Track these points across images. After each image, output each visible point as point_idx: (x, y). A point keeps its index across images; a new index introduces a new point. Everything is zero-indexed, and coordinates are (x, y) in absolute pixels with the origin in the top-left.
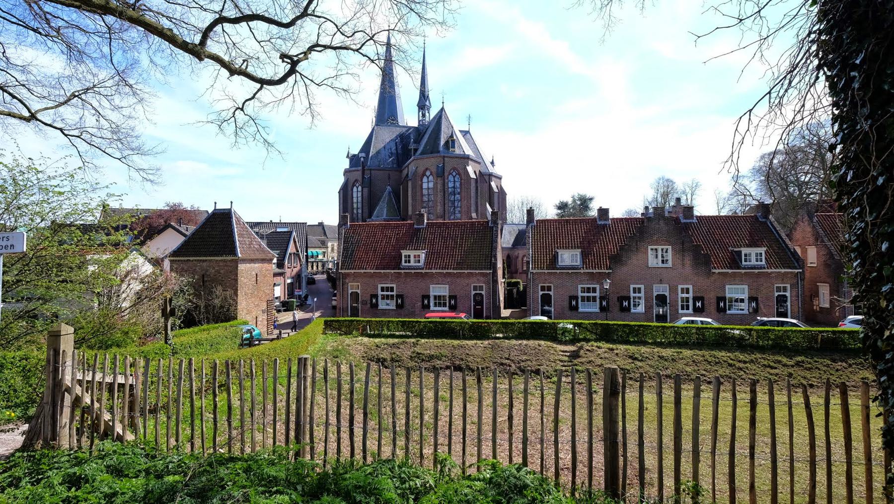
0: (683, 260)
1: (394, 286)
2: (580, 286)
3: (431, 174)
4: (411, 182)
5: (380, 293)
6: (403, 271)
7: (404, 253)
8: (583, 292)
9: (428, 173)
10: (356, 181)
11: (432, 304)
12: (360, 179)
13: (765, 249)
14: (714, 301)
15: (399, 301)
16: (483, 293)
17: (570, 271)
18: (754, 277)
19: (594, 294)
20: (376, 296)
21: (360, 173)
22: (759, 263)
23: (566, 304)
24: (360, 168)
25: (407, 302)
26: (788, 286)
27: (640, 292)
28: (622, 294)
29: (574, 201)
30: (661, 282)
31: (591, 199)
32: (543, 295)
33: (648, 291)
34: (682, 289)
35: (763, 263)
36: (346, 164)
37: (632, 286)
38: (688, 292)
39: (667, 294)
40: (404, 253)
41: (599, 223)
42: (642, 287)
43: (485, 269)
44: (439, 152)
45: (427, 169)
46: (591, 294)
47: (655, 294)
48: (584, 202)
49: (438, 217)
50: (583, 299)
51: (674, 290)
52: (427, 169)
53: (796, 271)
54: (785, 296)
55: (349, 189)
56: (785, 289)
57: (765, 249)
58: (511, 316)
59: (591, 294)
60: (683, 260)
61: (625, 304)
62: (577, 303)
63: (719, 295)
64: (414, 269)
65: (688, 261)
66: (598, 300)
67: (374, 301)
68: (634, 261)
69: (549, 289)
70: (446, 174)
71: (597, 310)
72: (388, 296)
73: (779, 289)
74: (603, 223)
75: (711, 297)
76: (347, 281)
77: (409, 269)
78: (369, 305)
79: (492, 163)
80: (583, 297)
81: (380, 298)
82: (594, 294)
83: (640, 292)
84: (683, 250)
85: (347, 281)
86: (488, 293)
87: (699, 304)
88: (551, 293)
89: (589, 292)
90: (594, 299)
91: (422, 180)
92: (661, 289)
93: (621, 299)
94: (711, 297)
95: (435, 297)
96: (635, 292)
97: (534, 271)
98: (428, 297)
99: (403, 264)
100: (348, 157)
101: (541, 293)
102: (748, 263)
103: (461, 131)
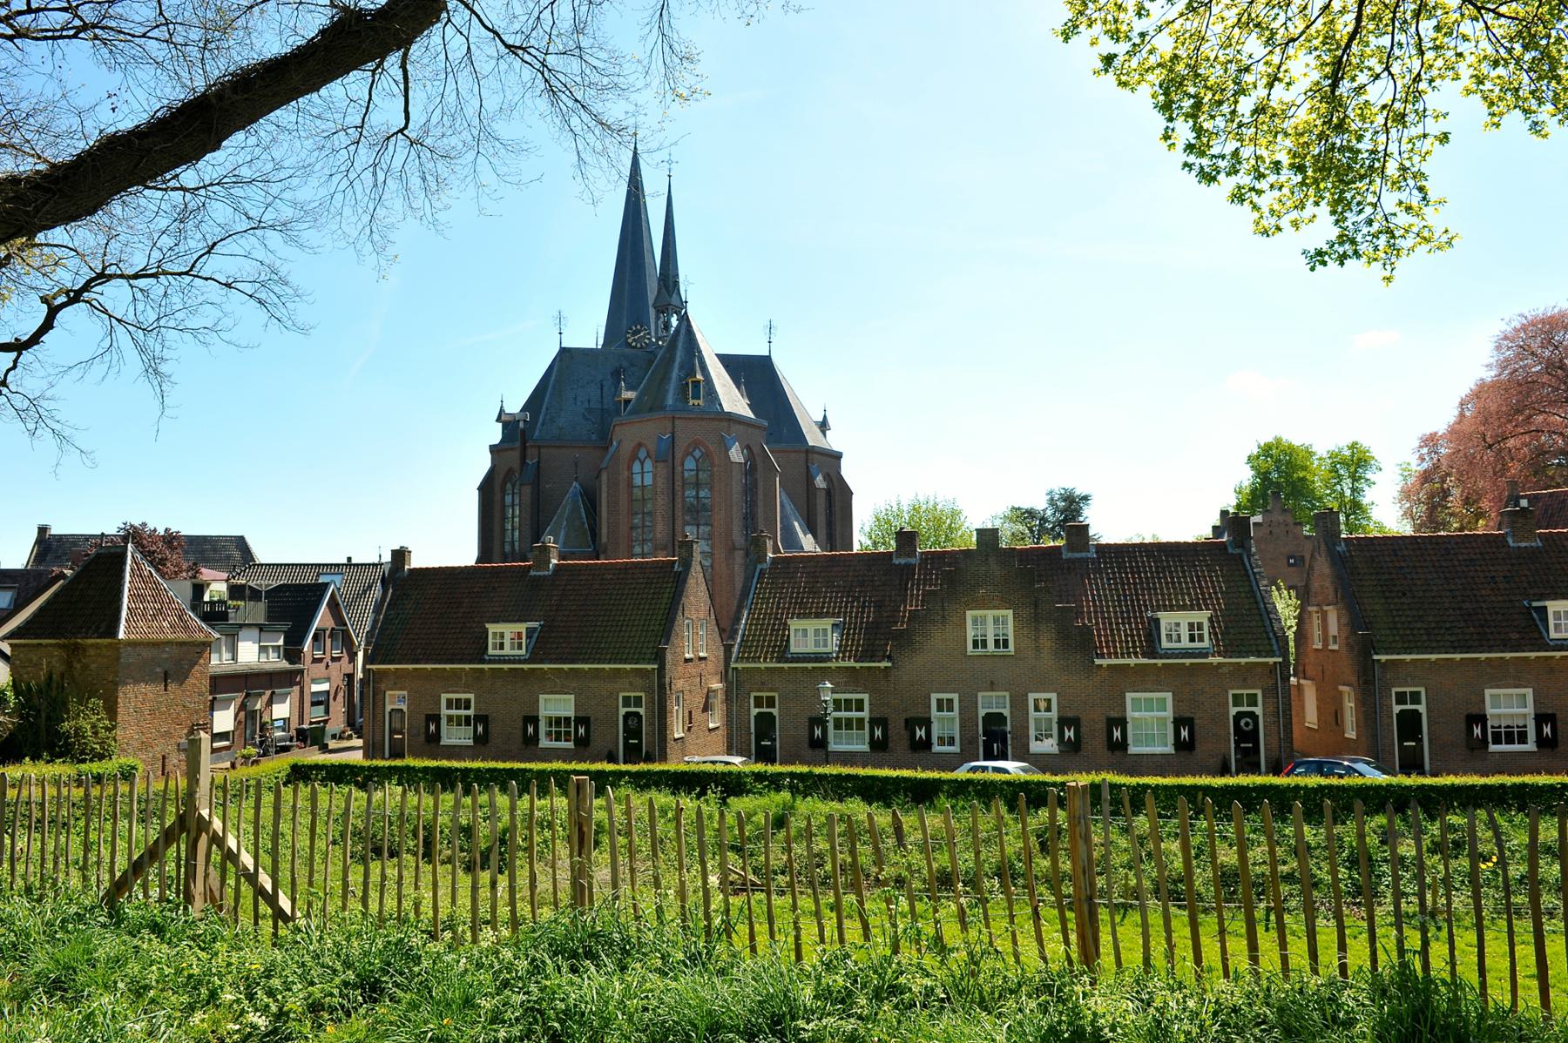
0: (1037, 639)
1: (471, 696)
2: (444, 697)
3: (649, 456)
4: (643, 469)
5: (445, 712)
6: (486, 666)
7: (492, 628)
8: (449, 706)
9: (642, 454)
10: (510, 471)
11: (542, 735)
12: (516, 465)
13: (1208, 613)
14: (1101, 726)
15: (878, 733)
16: (642, 711)
17: (810, 665)
18: (1182, 676)
19: (859, 714)
20: (436, 718)
21: (516, 454)
22: (1196, 645)
23: (805, 733)
24: (518, 444)
25: (494, 728)
26: (1259, 693)
27: (950, 709)
28: (912, 714)
29: (1052, 502)
30: (992, 686)
31: (1086, 498)
32: (627, 716)
33: (968, 707)
34: (449, 702)
35: (1206, 644)
36: (495, 434)
37: (934, 697)
38: (860, 708)
39: (1006, 712)
40: (492, 628)
41: (896, 561)
42: (955, 697)
43: (644, 661)
44: (663, 408)
45: (640, 445)
46: (854, 714)
47: (982, 712)
48: (1071, 506)
49: (656, 550)
50: (838, 724)
51: (1019, 704)
52: (640, 445)
53: (1271, 660)
54: (1417, 714)
55: (497, 489)
56: (1415, 698)
57: (1208, 613)
58: (743, 763)
59: (854, 714)
60: (1037, 639)
61: (920, 733)
62: (825, 732)
63: (1114, 714)
64: (509, 662)
65: (1047, 641)
66: (867, 726)
67: (530, 730)
68: (936, 641)
69: (771, 702)
70: (679, 455)
71: (866, 748)
72: (849, 722)
73: (1401, 699)
74: (903, 561)
75: (1093, 720)
76: (383, 686)
77: (499, 662)
78: (422, 738)
79: (824, 426)
80: (450, 719)
81: (444, 722)
82: (859, 714)
83: (950, 709)
84: (1036, 619)
85: (383, 686)
86: (649, 710)
87: (920, 733)
88: (775, 711)
89: (848, 709)
90: (860, 721)
91: (630, 468)
92: (992, 702)
93: (910, 724)
94: (1093, 720)
95: (550, 721)
96: (940, 709)
97: (740, 666)
98: (535, 720)
99: (490, 651)
100: (498, 420)
101: (755, 711)
102: (1174, 645)
103: (728, 361)
